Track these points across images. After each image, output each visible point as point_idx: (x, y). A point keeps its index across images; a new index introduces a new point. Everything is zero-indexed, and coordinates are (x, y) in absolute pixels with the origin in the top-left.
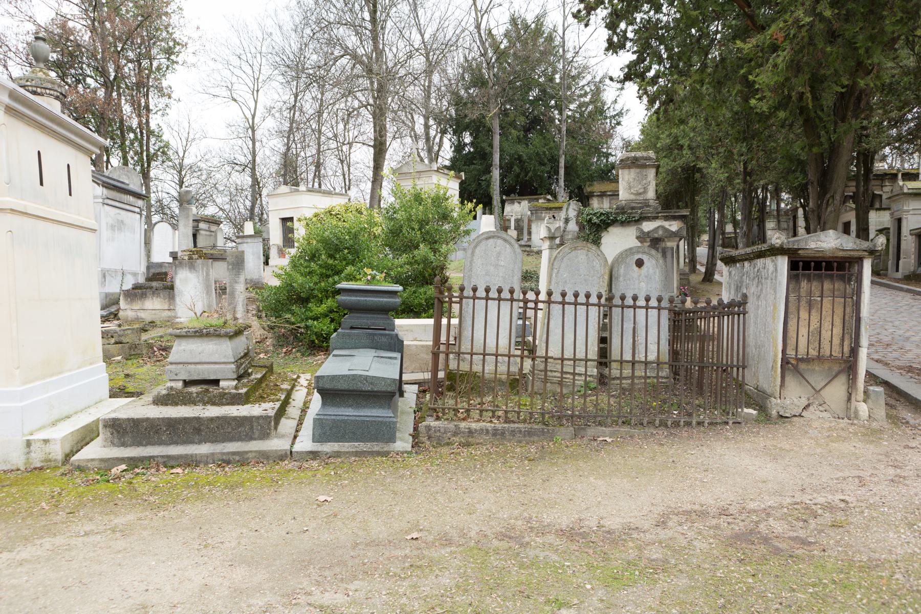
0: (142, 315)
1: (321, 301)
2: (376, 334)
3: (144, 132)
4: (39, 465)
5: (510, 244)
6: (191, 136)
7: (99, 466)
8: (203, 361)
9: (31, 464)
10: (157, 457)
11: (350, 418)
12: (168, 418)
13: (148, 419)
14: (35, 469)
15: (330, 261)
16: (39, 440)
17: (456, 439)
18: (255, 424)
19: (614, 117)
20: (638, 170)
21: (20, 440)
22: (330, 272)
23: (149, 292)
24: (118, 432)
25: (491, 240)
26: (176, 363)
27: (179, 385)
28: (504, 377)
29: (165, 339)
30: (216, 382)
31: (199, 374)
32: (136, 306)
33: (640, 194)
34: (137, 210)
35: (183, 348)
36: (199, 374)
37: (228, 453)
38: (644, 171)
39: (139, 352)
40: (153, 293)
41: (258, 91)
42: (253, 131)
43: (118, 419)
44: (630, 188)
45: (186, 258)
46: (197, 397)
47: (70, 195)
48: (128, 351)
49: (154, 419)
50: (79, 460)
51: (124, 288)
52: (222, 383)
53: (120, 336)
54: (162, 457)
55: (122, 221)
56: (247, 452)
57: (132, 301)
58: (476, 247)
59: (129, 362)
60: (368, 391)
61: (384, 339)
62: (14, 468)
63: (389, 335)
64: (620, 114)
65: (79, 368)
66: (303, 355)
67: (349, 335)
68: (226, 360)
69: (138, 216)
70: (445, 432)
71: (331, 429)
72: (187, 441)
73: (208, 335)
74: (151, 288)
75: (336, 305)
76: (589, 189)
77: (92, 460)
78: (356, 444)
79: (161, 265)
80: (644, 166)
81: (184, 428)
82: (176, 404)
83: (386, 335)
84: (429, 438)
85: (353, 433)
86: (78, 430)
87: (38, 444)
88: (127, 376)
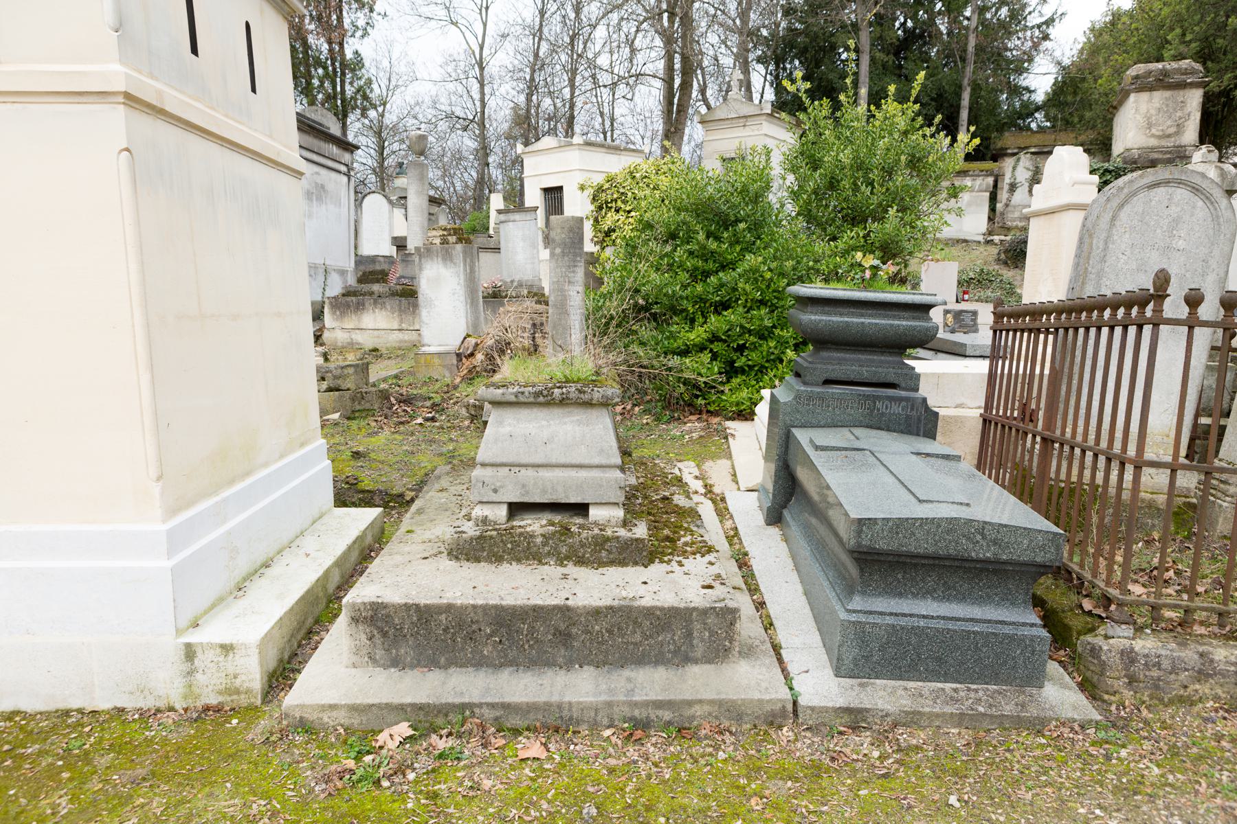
0: (358, 337)
1: (693, 321)
2: (878, 398)
3: (337, 64)
4: (213, 700)
5: (1208, 198)
6: (393, 83)
7: (347, 722)
8: (554, 461)
9: (198, 697)
10: (480, 705)
11: (933, 624)
12: (496, 607)
13: (449, 608)
14: (207, 709)
15: (713, 245)
16: (211, 646)
17: (1204, 689)
18: (697, 626)
19: (1039, 26)
20: (1168, 94)
21: (171, 644)
22: (711, 265)
23: (368, 301)
24: (385, 634)
25: (1161, 190)
26: (493, 465)
27: (503, 512)
28: (1161, 499)
29: (404, 382)
30: (581, 509)
31: (544, 491)
32: (350, 322)
33: (1169, 136)
34: (343, 169)
35: (506, 430)
36: (544, 491)
37: (646, 704)
38: (1180, 95)
39: (367, 406)
40: (375, 302)
41: (487, 8)
42: (482, 69)
43: (384, 606)
44: (1150, 126)
45: (437, 241)
46: (544, 544)
47: (254, 90)
48: (349, 403)
49: (464, 608)
50: (302, 706)
51: (328, 294)
52: (593, 512)
53: (335, 377)
54: (492, 706)
55: (323, 187)
56: (690, 703)
57: (343, 314)
58: (1121, 206)
59: (354, 424)
60: (986, 561)
61: (896, 409)
62: (161, 704)
63: (907, 399)
64: (1050, 22)
65: (282, 456)
66: (658, 419)
67: (822, 398)
68: (604, 462)
69: (345, 179)
70: (1174, 670)
71: (882, 648)
72: (538, 661)
73: (564, 402)
74: (371, 294)
75: (725, 327)
76: (999, 145)
77: (333, 707)
78: (948, 686)
79: (373, 259)
80: (1182, 86)
81: (532, 630)
82: (499, 559)
83: (901, 399)
84: (1132, 681)
85: (939, 660)
86: (292, 609)
87: (210, 655)
88: (357, 455)
